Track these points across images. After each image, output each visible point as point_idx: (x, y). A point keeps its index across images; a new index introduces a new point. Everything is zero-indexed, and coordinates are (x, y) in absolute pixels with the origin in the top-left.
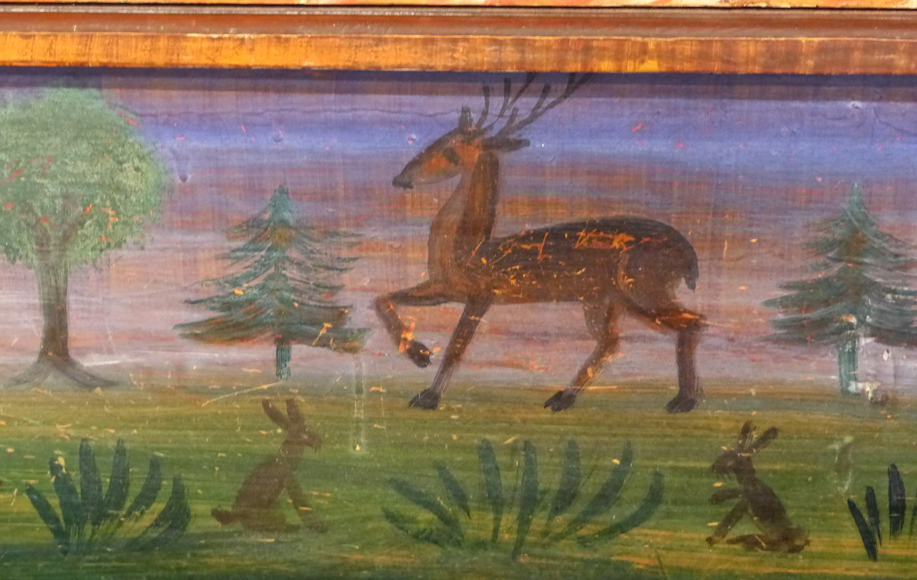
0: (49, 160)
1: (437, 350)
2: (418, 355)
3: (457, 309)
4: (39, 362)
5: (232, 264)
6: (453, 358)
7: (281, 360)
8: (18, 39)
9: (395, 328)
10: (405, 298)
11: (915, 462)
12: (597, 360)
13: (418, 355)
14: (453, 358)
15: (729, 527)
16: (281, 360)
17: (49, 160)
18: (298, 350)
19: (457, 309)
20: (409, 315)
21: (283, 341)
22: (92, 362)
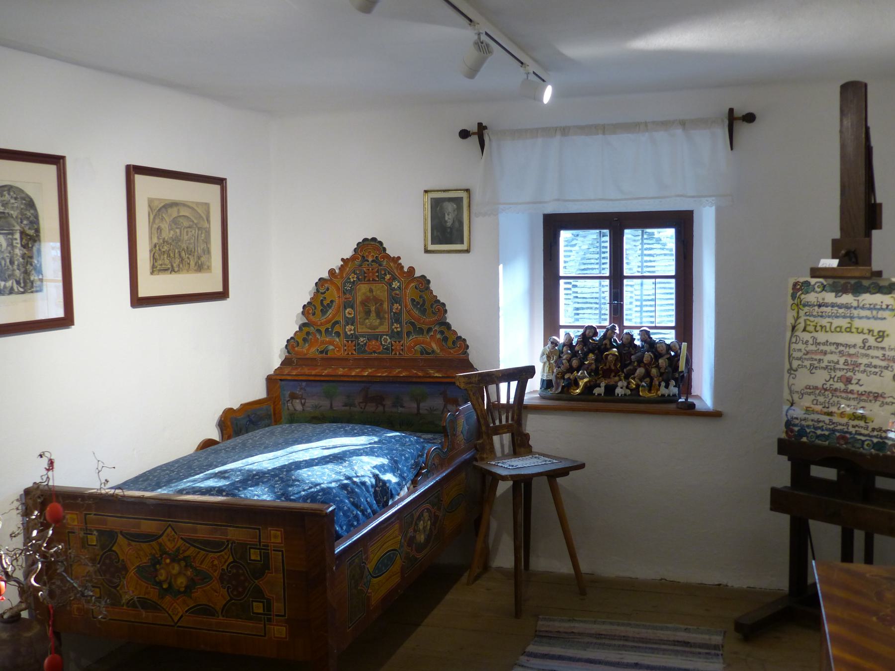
0: (87, 581)
1: (363, 407)
2: (361, 408)
3: (364, 404)
4: (600, 383)
5: (794, 317)
6: (364, 409)
7: (350, 408)
8: (319, 481)
9: (359, 405)
10: (360, 403)
11: (894, 399)
12: (377, 408)
13: (361, 408)
14: (364, 409)
15: (223, 419)
16: (350, 408)
17: (87, 581)
18: (351, 408)
19: (364, 404)
20: (361, 404)
21: (350, 407)
22: (335, 408)
